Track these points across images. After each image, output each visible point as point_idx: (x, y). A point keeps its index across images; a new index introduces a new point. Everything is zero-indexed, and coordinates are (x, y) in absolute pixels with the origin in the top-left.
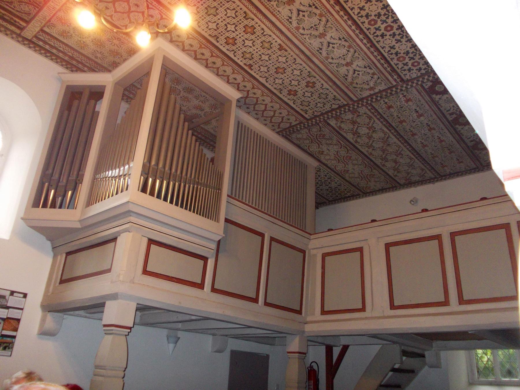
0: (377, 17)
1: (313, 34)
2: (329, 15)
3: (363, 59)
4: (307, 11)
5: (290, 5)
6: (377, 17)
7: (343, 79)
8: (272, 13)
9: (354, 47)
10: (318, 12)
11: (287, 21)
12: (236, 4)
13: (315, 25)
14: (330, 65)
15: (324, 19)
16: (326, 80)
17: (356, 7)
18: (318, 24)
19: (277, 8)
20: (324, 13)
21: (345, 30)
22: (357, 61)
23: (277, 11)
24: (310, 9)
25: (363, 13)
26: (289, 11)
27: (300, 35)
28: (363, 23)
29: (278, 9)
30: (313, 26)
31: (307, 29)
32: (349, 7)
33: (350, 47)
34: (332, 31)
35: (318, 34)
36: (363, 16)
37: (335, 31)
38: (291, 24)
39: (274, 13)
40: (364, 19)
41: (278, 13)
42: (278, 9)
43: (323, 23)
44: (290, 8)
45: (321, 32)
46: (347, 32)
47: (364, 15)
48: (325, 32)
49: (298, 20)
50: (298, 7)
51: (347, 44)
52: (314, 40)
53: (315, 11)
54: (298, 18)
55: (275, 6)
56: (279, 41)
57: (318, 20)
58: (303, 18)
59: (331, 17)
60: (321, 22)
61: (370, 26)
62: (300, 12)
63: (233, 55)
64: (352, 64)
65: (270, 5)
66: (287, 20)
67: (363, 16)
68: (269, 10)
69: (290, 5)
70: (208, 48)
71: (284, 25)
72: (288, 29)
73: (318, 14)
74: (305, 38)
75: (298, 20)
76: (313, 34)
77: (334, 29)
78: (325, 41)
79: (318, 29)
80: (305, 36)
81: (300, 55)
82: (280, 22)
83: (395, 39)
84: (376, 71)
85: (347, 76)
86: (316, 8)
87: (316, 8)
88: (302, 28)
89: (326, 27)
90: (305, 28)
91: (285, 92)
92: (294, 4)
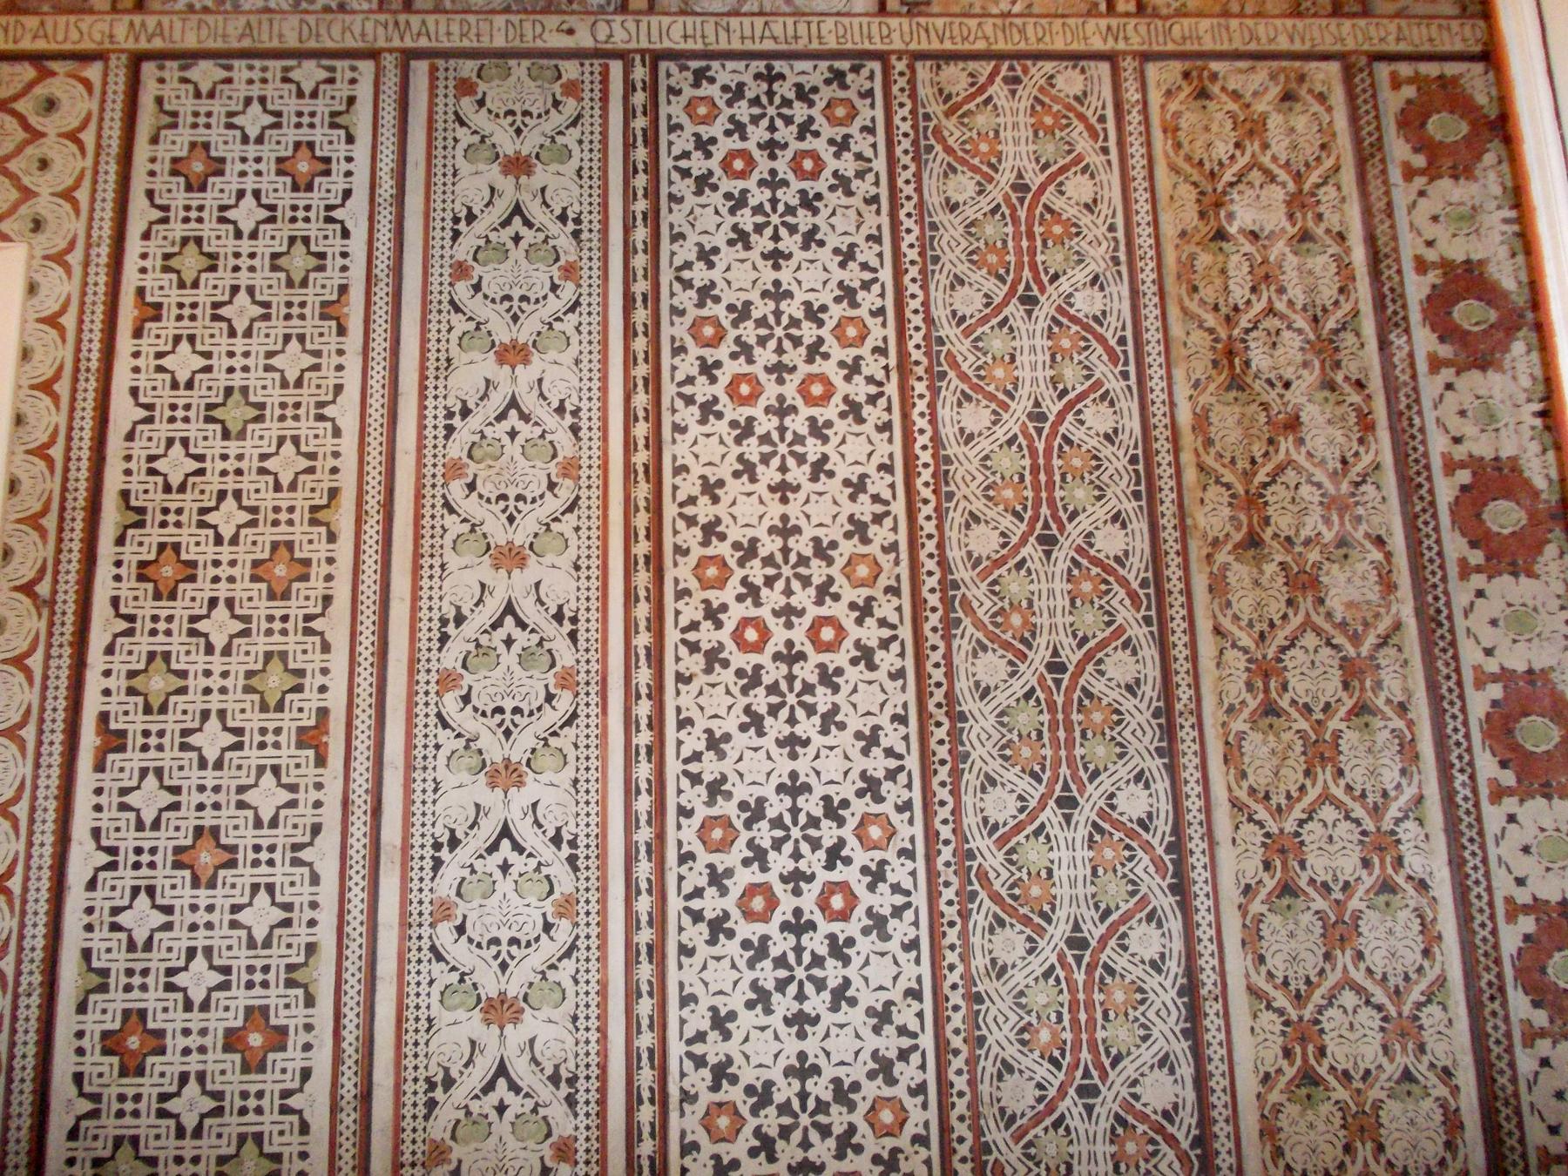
0: (739, 554)
1: (479, 744)
2: (594, 699)
3: (575, 1018)
4: (527, 1095)
5: (497, 568)
6: (739, 554)
7: (415, 1093)
8: (417, 555)
9: (584, 482)
10: (566, 656)
11: (436, 624)
12: (314, 889)
13: (526, 113)
14: (431, 730)
15: (564, 702)
16: (349, 1049)
17: (693, 238)
18: (534, 501)
19: (448, 551)
20: (582, 677)
21: (603, 814)
22: (554, 167)
23: (437, 562)
24: (550, 629)
25: (699, 275)
26: (487, 193)
27: (433, 720)
28: (681, 551)
29: (449, 556)
30: (508, 710)
31: (476, 709)
32: (679, 710)
33: (567, 907)
34: (556, 779)
35: (498, 759)
36: (700, 782)
37: (567, 785)
38: (447, 437)
39: (418, 775)
40: (687, 299)
41: (437, 571)
42: (460, 162)
43: (551, 717)
44: (487, 582)
45: (521, 341)
46: (603, 836)
47: (695, 173)
48: (525, 999)
49: (478, 646)
50: (515, 815)
51: (565, 882)
52: (465, 777)
53: (562, 647)
54: (484, 640)
55: (449, 537)
56: (336, 701)
57: (548, 285)
58: (502, 648)
59: (593, 710)
60: (548, 494)
61: (689, 342)
62: (517, 220)
63: (108, 639)
64: (522, 563)
65: (438, 522)
66: (428, 1080)
67: (700, 782)
68: (418, 537)
69: (497, 568)
70: (23, 913)
71: (413, 630)
72: (413, 661)
73: (562, 262)
74: (437, 747)
75: (478, 646)
76: (479, 744)
77: (569, 772)
78: (504, 586)
79: (515, 731)
80: (444, 736)
81: (372, 522)
82: (415, 609)
83: (734, 220)
84: (581, 1145)
85: (471, 217)
86: (573, 635)
87: (573, 635)
88: (458, 922)
89: (553, 140)
90: (475, 701)
91: (106, 1014)
92: (516, 572)
